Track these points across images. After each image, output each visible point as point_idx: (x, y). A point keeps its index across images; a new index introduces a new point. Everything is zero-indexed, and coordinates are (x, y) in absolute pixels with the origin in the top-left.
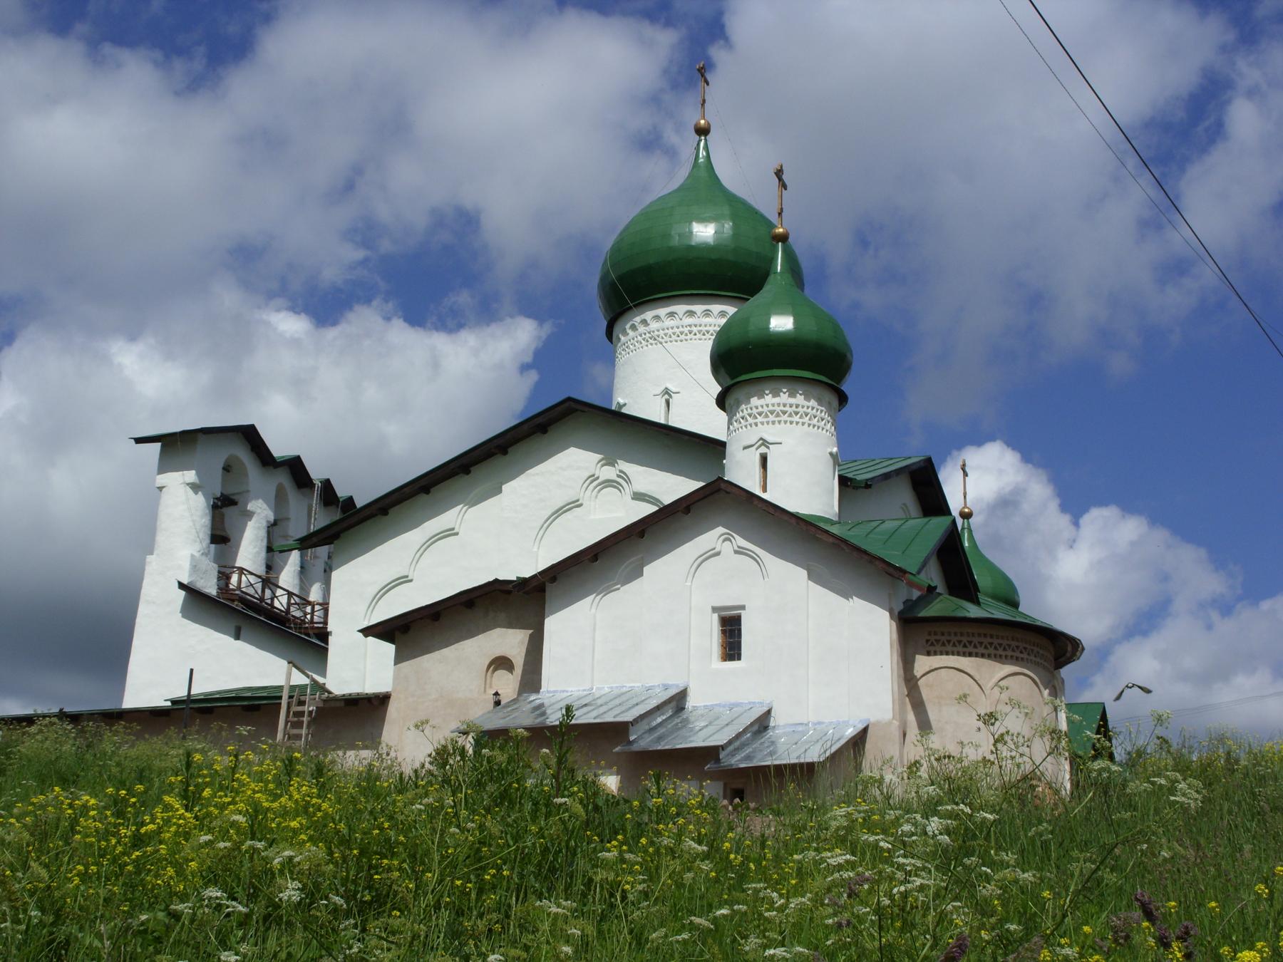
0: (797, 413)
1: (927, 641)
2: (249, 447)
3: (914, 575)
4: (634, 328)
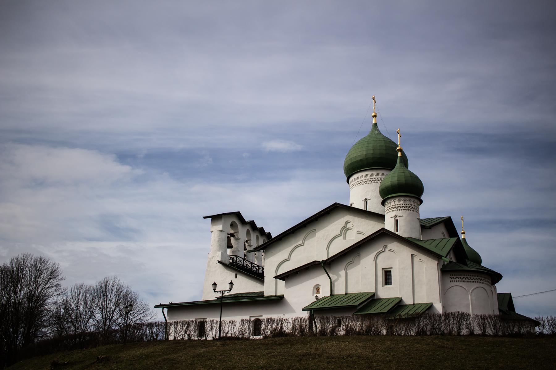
0: (407, 207)
1: (450, 278)
2: (238, 218)
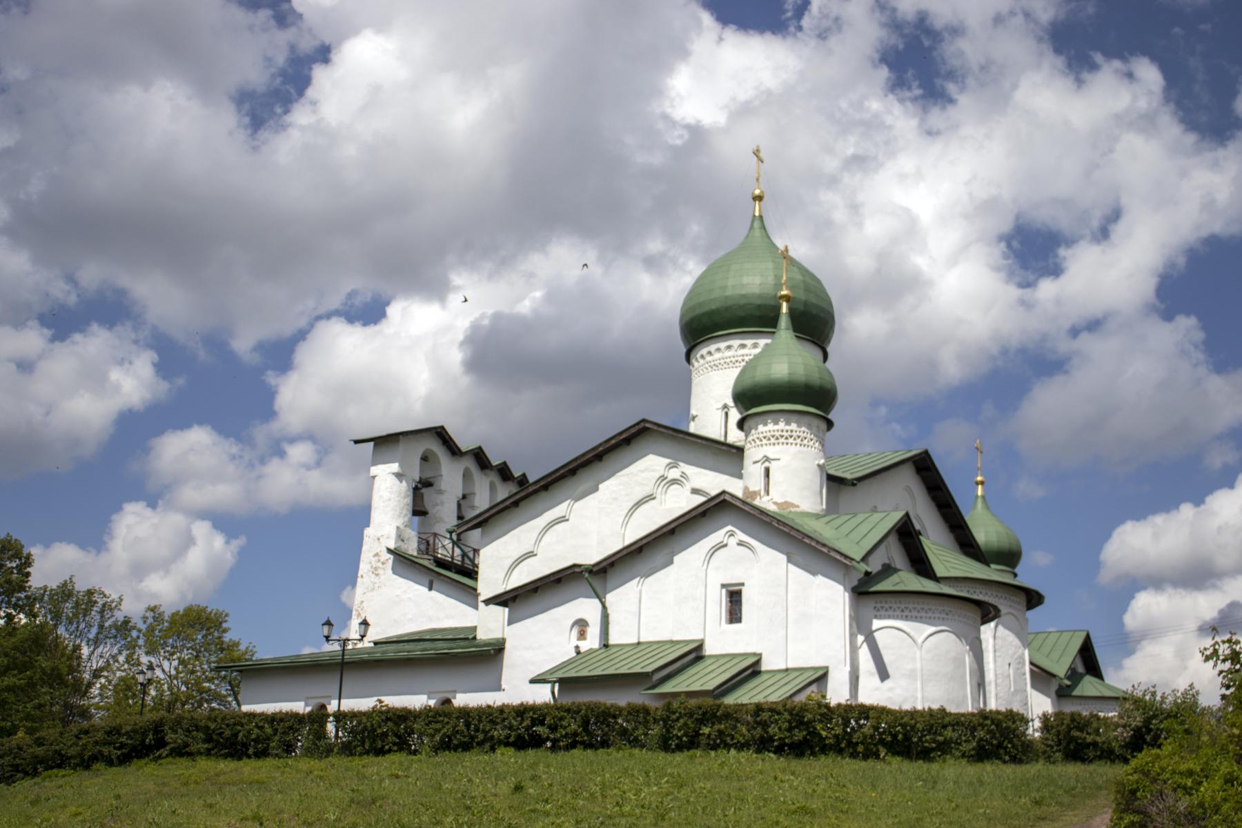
0: (791, 436)
1: (875, 608)
3: (858, 562)
4: (702, 357)
